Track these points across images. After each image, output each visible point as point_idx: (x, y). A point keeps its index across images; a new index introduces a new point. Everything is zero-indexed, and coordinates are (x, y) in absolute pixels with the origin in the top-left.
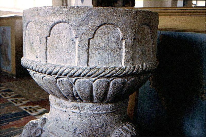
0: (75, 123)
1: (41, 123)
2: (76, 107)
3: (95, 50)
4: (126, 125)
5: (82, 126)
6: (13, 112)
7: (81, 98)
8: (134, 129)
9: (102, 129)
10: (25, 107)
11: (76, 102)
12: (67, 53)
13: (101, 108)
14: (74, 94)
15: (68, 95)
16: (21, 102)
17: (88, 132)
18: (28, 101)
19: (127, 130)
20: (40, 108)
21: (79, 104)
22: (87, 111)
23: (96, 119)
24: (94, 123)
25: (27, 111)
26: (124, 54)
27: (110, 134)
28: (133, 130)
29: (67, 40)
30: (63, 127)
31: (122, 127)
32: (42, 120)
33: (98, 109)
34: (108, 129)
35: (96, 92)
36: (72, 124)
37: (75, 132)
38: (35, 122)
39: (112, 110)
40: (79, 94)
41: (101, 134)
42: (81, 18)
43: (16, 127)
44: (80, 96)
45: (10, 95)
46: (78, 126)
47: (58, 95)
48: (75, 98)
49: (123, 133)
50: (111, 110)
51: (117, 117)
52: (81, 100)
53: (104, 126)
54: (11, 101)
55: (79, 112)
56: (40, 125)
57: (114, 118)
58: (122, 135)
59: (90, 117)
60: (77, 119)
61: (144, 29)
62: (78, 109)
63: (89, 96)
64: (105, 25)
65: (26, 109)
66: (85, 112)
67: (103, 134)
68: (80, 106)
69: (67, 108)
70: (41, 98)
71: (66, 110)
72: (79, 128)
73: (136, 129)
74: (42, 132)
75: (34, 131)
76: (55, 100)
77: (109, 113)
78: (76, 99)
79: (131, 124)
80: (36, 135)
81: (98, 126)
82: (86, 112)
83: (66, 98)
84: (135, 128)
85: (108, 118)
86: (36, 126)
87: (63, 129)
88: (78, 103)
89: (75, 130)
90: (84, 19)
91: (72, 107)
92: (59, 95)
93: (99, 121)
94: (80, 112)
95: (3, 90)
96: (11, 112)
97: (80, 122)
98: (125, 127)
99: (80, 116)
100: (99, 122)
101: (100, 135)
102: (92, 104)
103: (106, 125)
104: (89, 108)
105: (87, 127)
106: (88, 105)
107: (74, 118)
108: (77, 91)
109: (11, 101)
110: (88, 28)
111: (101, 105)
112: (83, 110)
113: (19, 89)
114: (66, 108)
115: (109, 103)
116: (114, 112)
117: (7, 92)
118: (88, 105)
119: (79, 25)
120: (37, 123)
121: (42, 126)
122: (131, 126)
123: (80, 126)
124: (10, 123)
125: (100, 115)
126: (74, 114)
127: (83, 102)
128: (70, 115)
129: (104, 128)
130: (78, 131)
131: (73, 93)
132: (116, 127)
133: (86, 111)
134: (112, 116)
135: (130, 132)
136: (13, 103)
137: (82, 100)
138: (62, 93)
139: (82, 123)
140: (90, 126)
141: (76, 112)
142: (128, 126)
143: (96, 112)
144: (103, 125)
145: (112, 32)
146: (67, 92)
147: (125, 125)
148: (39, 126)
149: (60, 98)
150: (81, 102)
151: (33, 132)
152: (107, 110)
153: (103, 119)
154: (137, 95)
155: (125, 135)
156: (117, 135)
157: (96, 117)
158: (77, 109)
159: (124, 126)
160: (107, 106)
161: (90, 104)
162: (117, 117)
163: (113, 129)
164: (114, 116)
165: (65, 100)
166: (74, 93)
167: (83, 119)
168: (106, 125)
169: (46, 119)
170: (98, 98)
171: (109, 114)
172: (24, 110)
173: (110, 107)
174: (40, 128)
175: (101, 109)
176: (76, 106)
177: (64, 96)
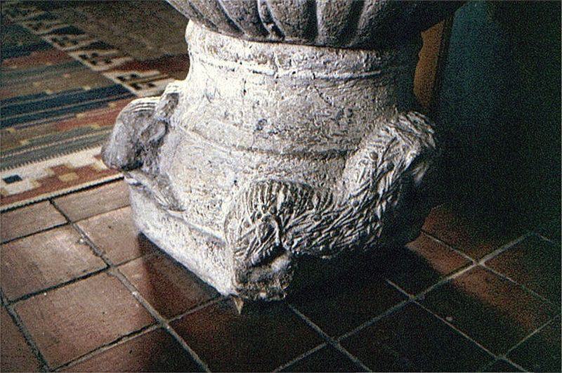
0: (260, 106)
1: (163, 106)
2: (263, 56)
4: (407, 118)
5: (280, 113)
6: (87, 88)
7: (279, 27)
8: (430, 130)
9: (339, 125)
10: (118, 74)
11: (266, 42)
13: (336, 63)
14: (261, 16)
15: (242, 19)
16: (108, 62)
17: (298, 132)
18: (128, 59)
19: (411, 133)
20: (161, 79)
21: (274, 47)
22: (296, 70)
23: (321, 95)
24: (316, 107)
25: (126, 86)
27: (361, 139)
28: (427, 133)
30: (226, 115)
31: (398, 124)
32: (167, 97)
33: (329, 65)
34: (354, 124)
35: (326, 9)
36: (254, 107)
37: (260, 128)
38: (148, 103)
39: (371, 70)
40: (274, 15)
41: (335, 139)
43: (95, 126)
44: (278, 23)
45: (75, 43)
47: (212, 20)
48: (262, 26)
49: (399, 139)
50: (366, 72)
51: (383, 92)
52: (280, 38)
53: (345, 116)
54: (80, 60)
55: (272, 73)
56: (161, 111)
57: (375, 95)
58: (394, 143)
59: (304, 89)
60: (266, 92)
62: (271, 64)
63: (303, 20)
65: (121, 78)
66: (291, 74)
67: (340, 138)
68: (275, 55)
69: (239, 61)
70: (166, 51)
71: (236, 65)
72: (273, 120)
73: (436, 133)
74: (167, 131)
75: (146, 126)
76: (204, 38)
77: (361, 78)
78: (265, 33)
79: (423, 116)
80: (151, 139)
81: (326, 116)
82: (294, 73)
83: (235, 30)
84: (432, 127)
85: (358, 92)
86: (151, 112)
87: (226, 120)
88: (269, 46)
89: (261, 123)
91: (252, 57)
92: (214, 18)
93: (332, 100)
94: (277, 71)
95: (56, 28)
96: (79, 87)
97: (275, 102)
98: (406, 123)
99: (276, 86)
100: (331, 104)
101: (332, 139)
102: (310, 50)
103: (349, 114)
104: (303, 60)
105: (296, 118)
106: (300, 52)
107: (259, 90)
108: (269, 6)
109: (80, 60)
111: (337, 53)
112: (286, 66)
113: (101, 26)
114: (236, 61)
115: (363, 49)
116: (374, 77)
117: (68, 33)
118: (299, 51)
120: (154, 107)
121: (167, 114)
122: (423, 121)
123: (275, 113)
124: (80, 115)
125: (335, 85)
126: (259, 78)
127: (287, 42)
128: (245, 82)
129: (343, 121)
131: (256, 9)
132: (378, 121)
133: (293, 71)
134: (369, 88)
135: (420, 138)
136: (86, 63)
137: (284, 37)
138: (223, 10)
139: (281, 105)
140: (303, 115)
142: (415, 121)
143: (322, 74)
144: (342, 113)
146: (239, 9)
147: (405, 119)
148: (158, 115)
149: (216, 31)
150: (278, 42)
151: (142, 129)
152: (356, 68)
153: (342, 96)
154: (447, 33)
155: (404, 143)
156: (381, 141)
158: (268, 62)
159: (402, 122)
160: (356, 58)
161: (307, 48)
162: (383, 92)
163: (370, 126)
164: (376, 86)
165: (234, 37)
166: (260, 10)
167: (283, 94)
168: (349, 114)
169: (177, 94)
170: (329, 30)
171: (362, 82)
172: (118, 82)
173: (366, 61)
174: (162, 119)
175: (337, 65)
176: (265, 54)
177: (231, 21)
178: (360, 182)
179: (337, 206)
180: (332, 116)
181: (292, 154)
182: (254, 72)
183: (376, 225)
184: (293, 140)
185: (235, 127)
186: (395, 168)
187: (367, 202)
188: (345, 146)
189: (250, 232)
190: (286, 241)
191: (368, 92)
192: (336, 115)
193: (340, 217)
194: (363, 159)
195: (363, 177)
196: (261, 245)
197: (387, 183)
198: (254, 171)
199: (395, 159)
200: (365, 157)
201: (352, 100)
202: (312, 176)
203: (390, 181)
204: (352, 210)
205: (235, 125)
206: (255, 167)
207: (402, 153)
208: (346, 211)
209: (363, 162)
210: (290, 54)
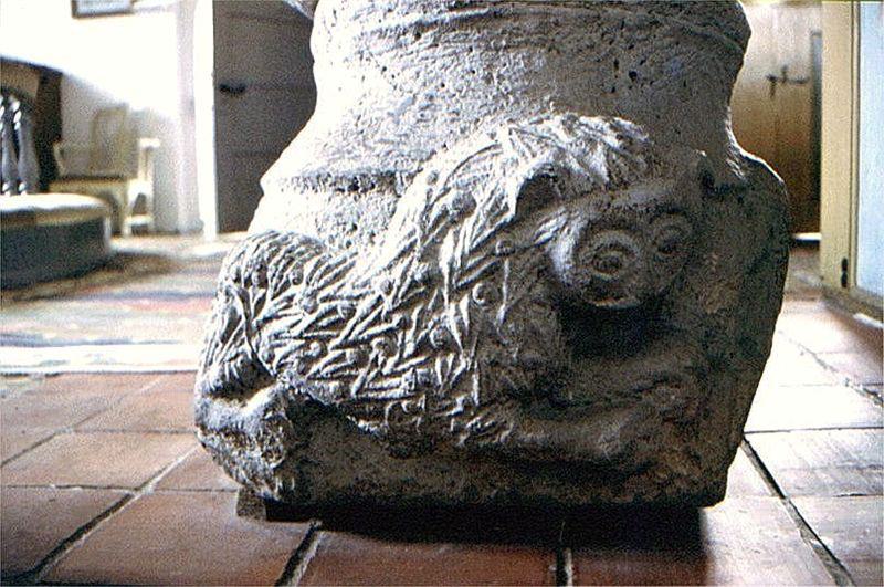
183: (455, 363)
186: (476, 211)
187: (410, 287)
188: (393, 163)
191: (474, 59)
193: (358, 314)
196: (222, 349)
197: (460, 244)
199: (479, 187)
201: (437, 77)
202: (330, 224)
203: (468, 244)
204: (380, 299)
207: (499, 172)
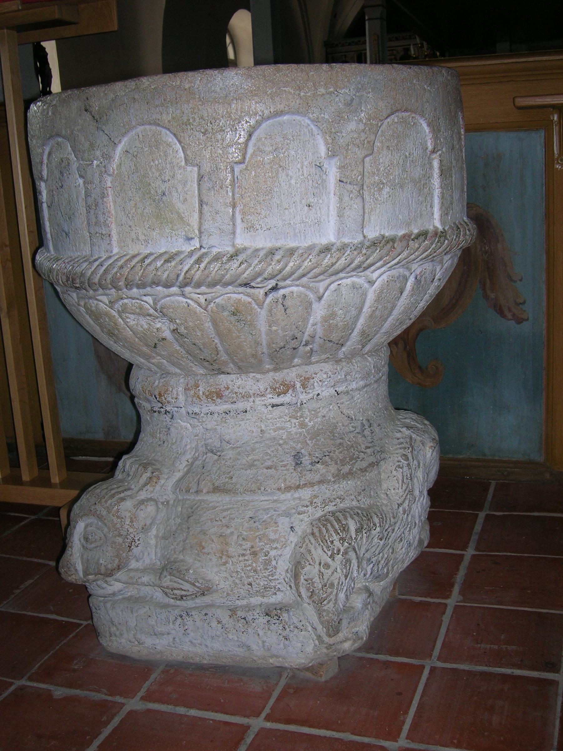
3: (380, 190)
12: (306, 208)
26: (437, 193)
29: (304, 168)
33: (348, 377)
41: (369, 451)
42: (342, 99)
46: (299, 445)
49: (414, 436)
53: (367, 427)
61: (124, 184)
64: (397, 114)
66: (315, 396)
90: (352, 100)
100: (352, 419)
110: (361, 127)
119: (339, 117)
129: (367, 432)
130: (307, 458)
133: (317, 393)
141: (285, 402)
145: (412, 133)
157: (344, 405)
178: (402, 488)
179: (392, 519)
180: (357, 431)
181: (340, 477)
182: (273, 407)
184: (336, 463)
185: (269, 470)
189: (333, 573)
190: (363, 572)
192: (359, 428)
194: (398, 464)
195: (403, 481)
198: (310, 508)
200: (399, 461)
205: (268, 468)
206: (309, 504)
208: (399, 522)
209: (399, 466)
210: (314, 375)
